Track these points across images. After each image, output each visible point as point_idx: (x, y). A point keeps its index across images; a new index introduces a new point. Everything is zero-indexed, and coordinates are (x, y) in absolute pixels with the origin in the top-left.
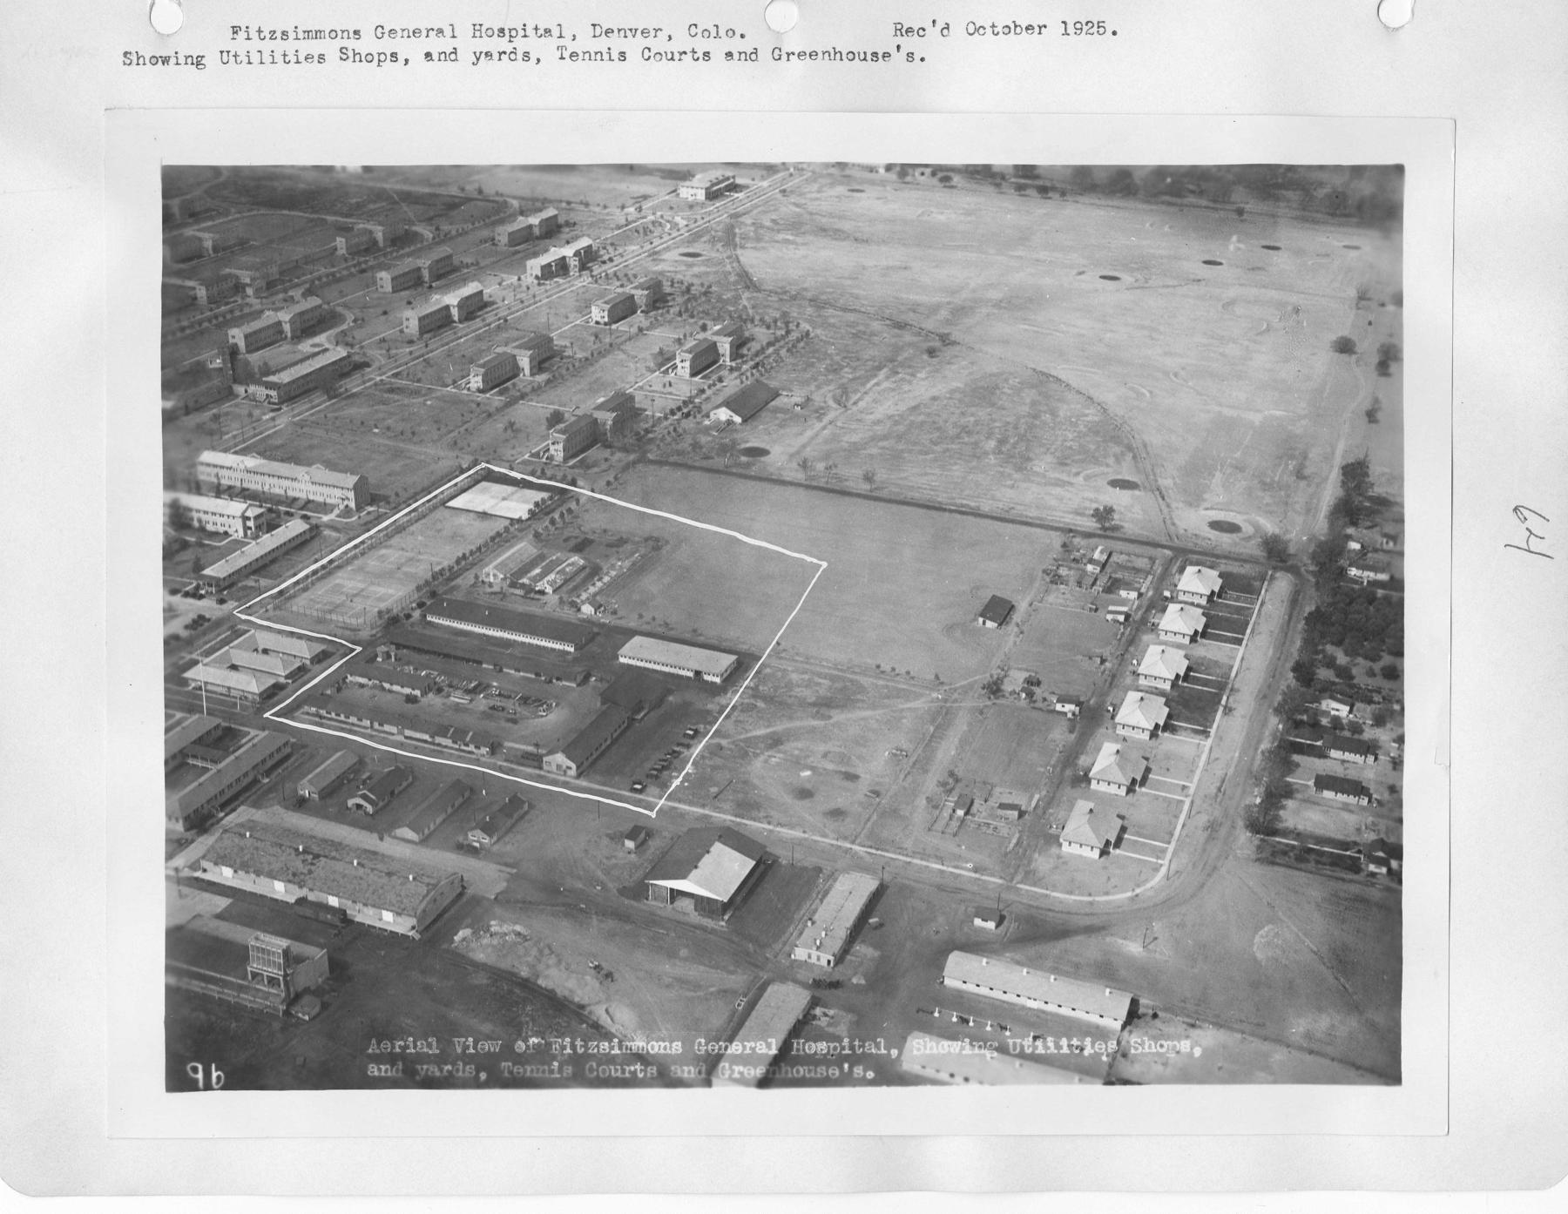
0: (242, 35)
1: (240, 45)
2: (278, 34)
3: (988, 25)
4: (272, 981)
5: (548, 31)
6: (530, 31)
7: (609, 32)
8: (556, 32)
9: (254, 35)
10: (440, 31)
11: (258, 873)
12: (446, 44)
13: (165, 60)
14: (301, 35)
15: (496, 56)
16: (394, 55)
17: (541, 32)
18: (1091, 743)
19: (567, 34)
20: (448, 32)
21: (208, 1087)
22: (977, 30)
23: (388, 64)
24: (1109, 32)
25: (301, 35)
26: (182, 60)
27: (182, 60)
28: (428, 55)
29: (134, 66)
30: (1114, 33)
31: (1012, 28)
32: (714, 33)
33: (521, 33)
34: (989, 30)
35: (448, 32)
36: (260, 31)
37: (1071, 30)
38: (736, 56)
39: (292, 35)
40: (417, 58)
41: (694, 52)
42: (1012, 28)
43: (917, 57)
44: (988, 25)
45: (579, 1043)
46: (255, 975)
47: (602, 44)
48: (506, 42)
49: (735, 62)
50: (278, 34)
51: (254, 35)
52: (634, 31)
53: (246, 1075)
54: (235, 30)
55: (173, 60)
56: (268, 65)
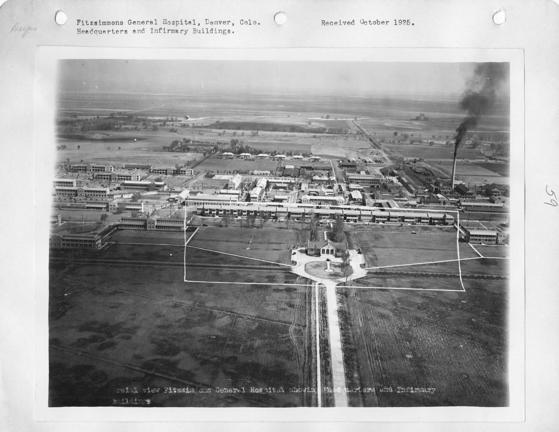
0: (81, 23)
2: (94, 23)
3: (368, 21)
5: (190, 22)
6: (184, 23)
8: (192, 22)
9: (85, 23)
10: (151, 22)
14: (101, 23)
16: (229, 31)
17: (188, 22)
19: (197, 23)
20: (154, 22)
21: (328, 402)
22: (364, 23)
24: (411, 24)
25: (101, 23)
27: (218, 31)
28: (134, 31)
29: (214, 34)
31: (377, 22)
32: (249, 23)
33: (180, 23)
34: (368, 23)
35: (154, 22)
36: (186, 21)
37: (398, 23)
38: (137, 31)
39: (98, 23)
40: (191, 31)
42: (377, 22)
43: (231, 31)
44: (368, 21)
45: (274, 389)
47: (210, 27)
48: (174, 27)
49: (136, 34)
51: (85, 23)
52: (220, 22)
53: (354, 406)
56: (206, 34)
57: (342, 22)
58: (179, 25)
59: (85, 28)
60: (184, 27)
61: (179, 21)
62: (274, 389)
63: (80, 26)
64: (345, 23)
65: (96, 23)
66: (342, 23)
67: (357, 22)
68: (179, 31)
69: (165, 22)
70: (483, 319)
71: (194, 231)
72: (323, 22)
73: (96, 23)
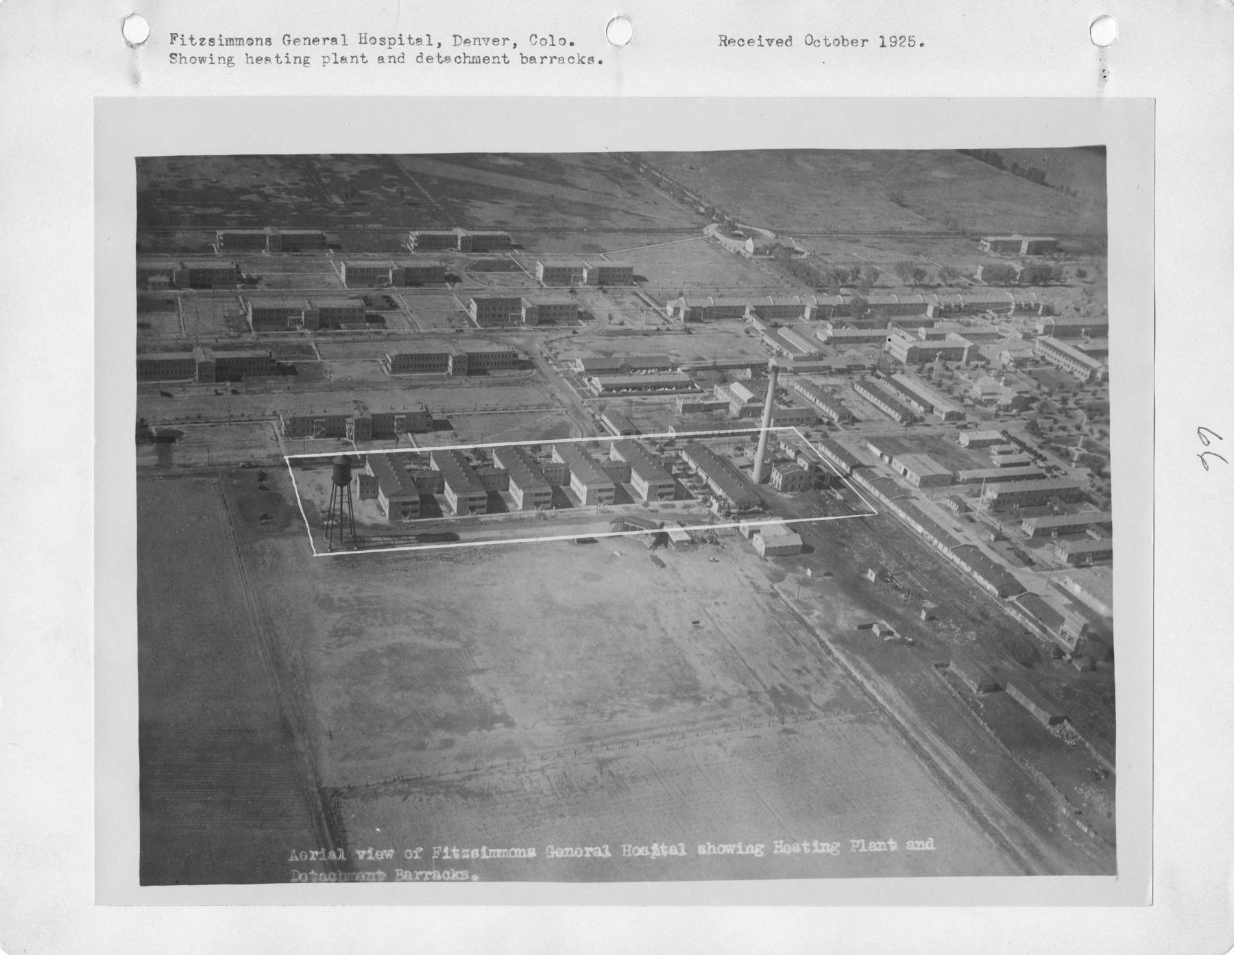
1: (177, 47)
2: (207, 41)
4: (1071, 639)
6: (405, 40)
7: (467, 41)
9: (187, 41)
10: (334, 40)
11: (1095, 596)
12: (397, 51)
13: (202, 60)
15: (539, 60)
18: (271, 382)
19: (435, 42)
20: (340, 40)
22: (813, 42)
23: (331, 66)
25: (224, 42)
26: (216, 60)
27: (292, 60)
30: (600, 62)
32: (549, 42)
33: (398, 41)
34: (823, 42)
36: (192, 39)
38: (349, 59)
39: (217, 42)
40: (373, 60)
41: (439, 56)
43: (596, 60)
45: (455, 850)
46: (1063, 633)
47: (302, 50)
49: (386, 65)
50: (207, 41)
51: (187, 41)
54: (174, 36)
55: (209, 60)
57: (763, 39)
58: (396, 46)
59: (189, 51)
60: (227, 51)
61: (397, 37)
62: (455, 850)
63: (177, 47)
64: (770, 41)
65: (212, 40)
66: (764, 42)
67: (798, 41)
68: (539, 60)
69: (287, 39)
70: (774, 641)
71: (476, 449)
72: (726, 41)
73: (212, 40)
